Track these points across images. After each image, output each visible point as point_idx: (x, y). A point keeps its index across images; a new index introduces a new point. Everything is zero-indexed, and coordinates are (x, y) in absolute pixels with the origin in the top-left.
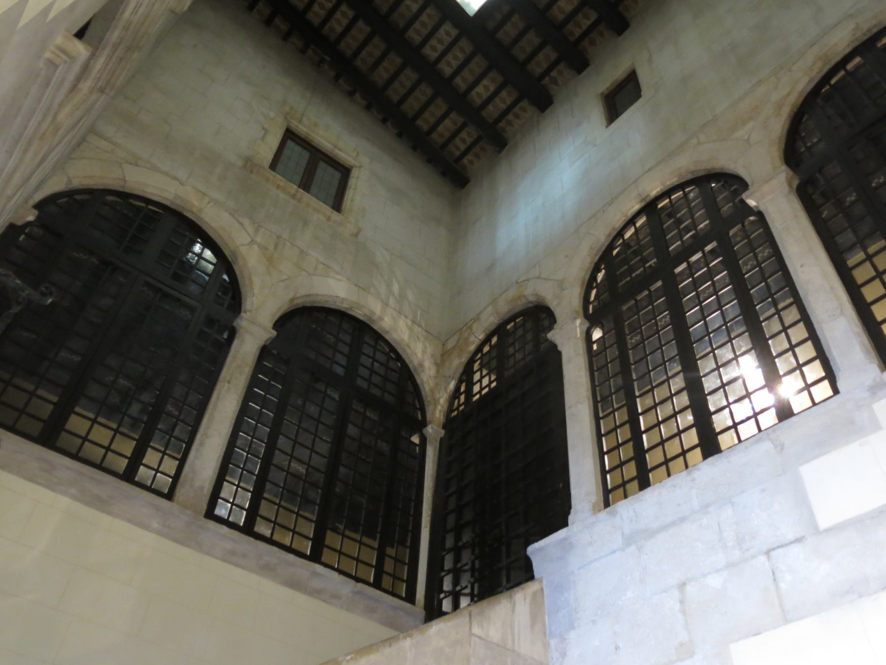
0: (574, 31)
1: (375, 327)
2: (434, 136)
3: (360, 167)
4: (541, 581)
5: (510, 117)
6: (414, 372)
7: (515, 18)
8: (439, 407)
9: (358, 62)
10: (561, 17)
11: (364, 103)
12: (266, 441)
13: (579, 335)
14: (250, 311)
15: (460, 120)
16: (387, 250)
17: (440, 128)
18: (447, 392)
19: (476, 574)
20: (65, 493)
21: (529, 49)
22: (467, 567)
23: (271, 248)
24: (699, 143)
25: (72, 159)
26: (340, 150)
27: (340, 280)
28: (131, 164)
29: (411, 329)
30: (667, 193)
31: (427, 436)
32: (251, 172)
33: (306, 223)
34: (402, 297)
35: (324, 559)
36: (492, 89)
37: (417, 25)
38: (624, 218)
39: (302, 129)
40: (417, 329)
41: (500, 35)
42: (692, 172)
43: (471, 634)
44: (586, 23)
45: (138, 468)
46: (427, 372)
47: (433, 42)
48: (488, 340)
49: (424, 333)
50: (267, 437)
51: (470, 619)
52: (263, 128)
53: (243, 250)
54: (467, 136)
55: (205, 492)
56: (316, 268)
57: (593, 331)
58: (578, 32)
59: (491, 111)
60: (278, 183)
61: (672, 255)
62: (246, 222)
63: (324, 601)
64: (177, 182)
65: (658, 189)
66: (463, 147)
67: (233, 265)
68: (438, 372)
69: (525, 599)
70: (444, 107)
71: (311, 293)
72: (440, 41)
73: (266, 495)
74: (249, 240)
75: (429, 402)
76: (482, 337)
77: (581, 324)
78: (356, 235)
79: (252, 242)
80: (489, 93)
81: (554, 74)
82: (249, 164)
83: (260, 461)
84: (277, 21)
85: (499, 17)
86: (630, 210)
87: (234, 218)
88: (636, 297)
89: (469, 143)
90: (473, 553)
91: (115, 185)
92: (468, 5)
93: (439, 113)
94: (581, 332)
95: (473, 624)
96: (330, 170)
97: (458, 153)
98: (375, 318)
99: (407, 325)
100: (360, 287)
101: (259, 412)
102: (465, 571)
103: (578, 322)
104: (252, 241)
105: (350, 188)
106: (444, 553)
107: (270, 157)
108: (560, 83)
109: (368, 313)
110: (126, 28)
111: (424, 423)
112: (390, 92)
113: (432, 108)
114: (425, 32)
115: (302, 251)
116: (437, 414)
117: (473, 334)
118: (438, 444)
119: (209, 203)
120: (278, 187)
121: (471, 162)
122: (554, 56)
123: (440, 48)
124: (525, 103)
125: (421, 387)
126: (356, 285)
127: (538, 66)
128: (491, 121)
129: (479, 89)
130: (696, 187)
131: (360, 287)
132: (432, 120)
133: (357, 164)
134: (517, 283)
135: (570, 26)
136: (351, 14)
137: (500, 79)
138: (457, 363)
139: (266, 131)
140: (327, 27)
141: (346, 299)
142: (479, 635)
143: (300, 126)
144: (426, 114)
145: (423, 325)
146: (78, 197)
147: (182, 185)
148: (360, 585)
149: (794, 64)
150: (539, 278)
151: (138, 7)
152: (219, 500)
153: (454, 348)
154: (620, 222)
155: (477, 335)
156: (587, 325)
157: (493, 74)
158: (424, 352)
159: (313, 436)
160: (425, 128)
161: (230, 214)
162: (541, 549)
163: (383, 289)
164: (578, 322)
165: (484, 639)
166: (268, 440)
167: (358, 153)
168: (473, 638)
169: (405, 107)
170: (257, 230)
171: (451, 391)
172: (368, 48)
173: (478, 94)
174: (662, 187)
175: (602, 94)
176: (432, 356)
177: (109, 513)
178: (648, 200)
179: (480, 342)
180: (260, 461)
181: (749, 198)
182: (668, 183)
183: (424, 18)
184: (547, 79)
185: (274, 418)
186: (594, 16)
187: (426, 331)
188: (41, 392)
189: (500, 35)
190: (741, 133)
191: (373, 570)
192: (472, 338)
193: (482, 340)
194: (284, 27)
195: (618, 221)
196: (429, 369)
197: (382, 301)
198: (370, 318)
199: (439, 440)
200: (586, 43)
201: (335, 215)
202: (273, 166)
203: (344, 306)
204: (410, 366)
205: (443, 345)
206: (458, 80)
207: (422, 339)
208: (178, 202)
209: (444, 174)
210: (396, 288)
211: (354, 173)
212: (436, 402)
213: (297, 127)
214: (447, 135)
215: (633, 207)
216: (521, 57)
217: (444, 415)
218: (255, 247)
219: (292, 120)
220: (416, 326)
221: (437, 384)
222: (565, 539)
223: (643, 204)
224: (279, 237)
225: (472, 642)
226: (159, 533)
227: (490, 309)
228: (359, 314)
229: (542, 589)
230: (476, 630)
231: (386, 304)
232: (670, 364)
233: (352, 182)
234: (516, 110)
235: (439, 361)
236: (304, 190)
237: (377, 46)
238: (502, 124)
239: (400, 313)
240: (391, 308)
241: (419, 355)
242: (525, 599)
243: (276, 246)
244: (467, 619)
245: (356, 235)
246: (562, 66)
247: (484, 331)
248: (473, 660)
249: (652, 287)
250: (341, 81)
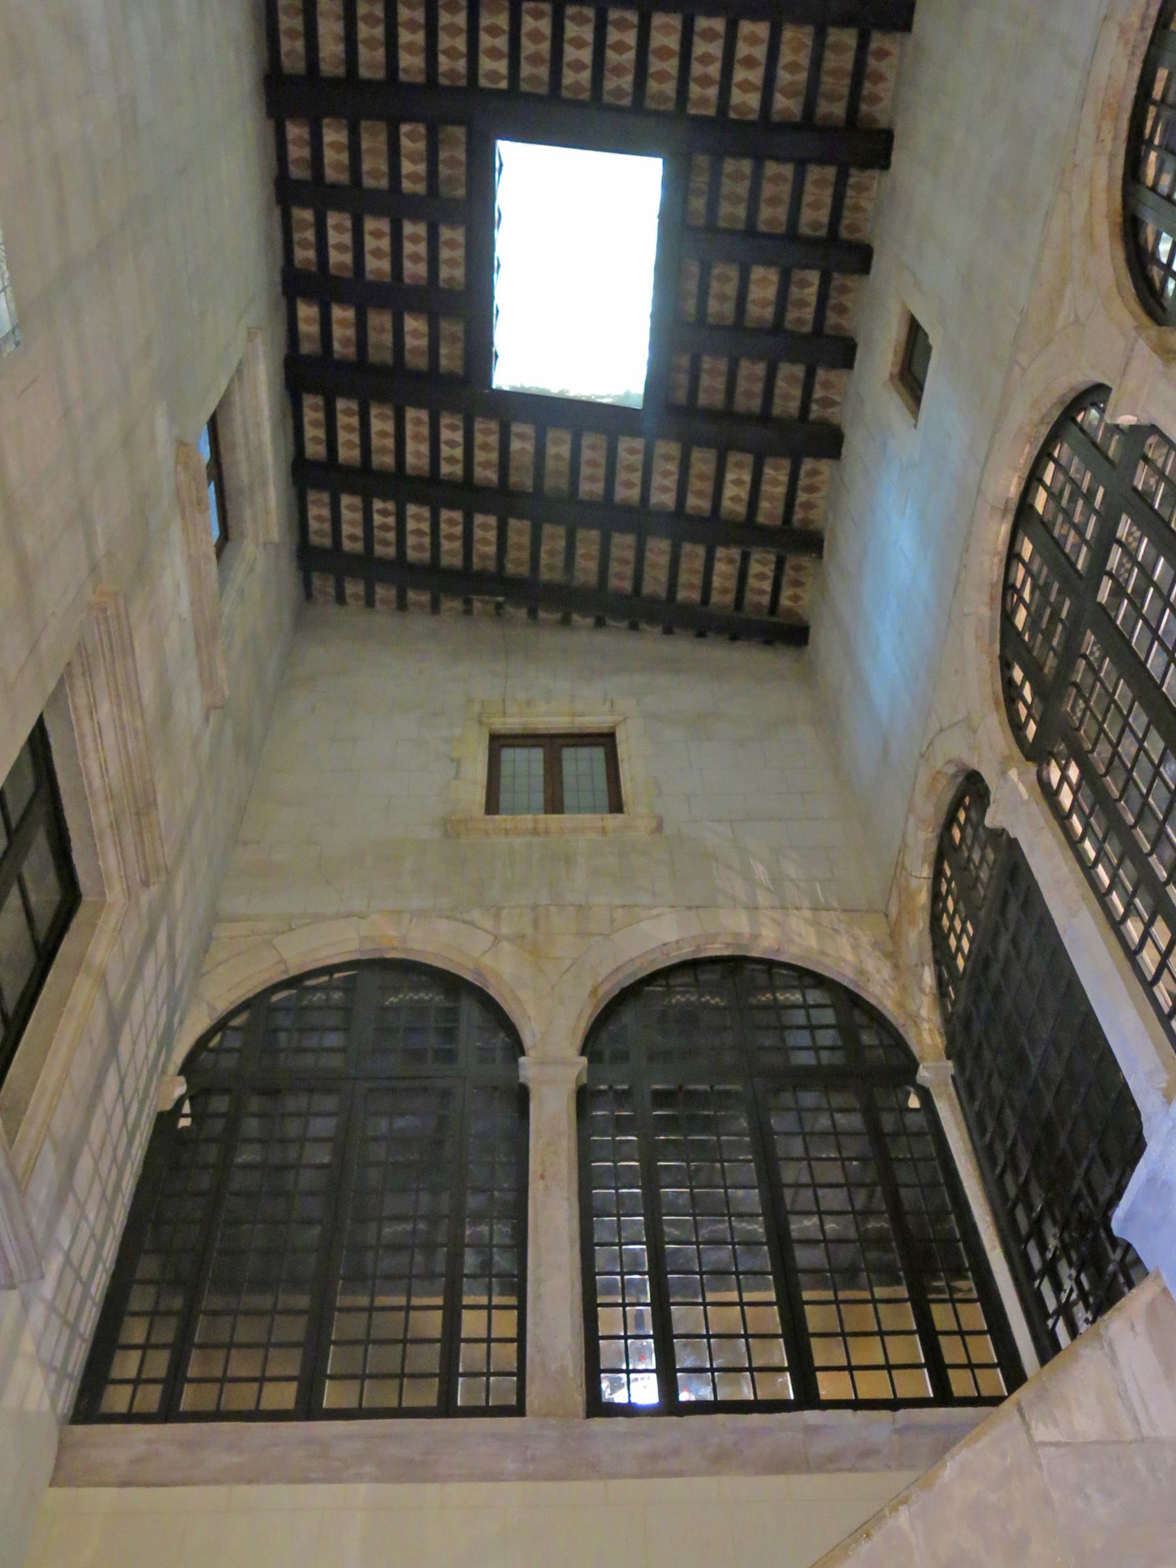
0: (801, 316)
1: (755, 954)
2: (715, 598)
3: (625, 720)
4: (1158, 1276)
5: (802, 497)
6: (856, 990)
7: (707, 363)
8: (926, 1026)
9: (545, 575)
10: (769, 313)
11: (590, 621)
12: (644, 1240)
13: (1026, 796)
14: (534, 1047)
15: (735, 553)
16: (719, 821)
17: (717, 582)
18: (926, 994)
19: (1091, 1300)
20: (359, 1478)
21: (758, 387)
22: (1074, 1296)
23: (529, 930)
24: (1024, 370)
25: (203, 975)
26: (582, 715)
27: (658, 916)
28: (283, 932)
29: (816, 924)
30: (1033, 479)
31: (927, 1085)
32: (458, 836)
33: (569, 860)
34: (777, 879)
35: (825, 1393)
36: (747, 478)
37: (585, 471)
38: (996, 560)
39: (512, 723)
40: (825, 917)
41: (703, 399)
42: (1042, 421)
43: (1035, 1446)
44: (811, 293)
45: (777, 1295)
46: (877, 976)
47: (622, 476)
48: (938, 873)
49: (843, 917)
50: (644, 1232)
51: (1022, 1416)
52: (452, 760)
53: (487, 961)
54: (761, 566)
55: (571, 1374)
56: (612, 920)
57: (1048, 773)
58: (809, 313)
59: (770, 510)
60: (504, 826)
61: (1084, 575)
62: (476, 915)
63: (852, 1470)
64: (355, 919)
65: (1015, 480)
66: (767, 586)
67: (486, 990)
68: (896, 967)
69: (1132, 1327)
70: (701, 551)
71: (619, 964)
72: (630, 468)
73: (807, 1295)
74: (491, 938)
75: (904, 1025)
76: (926, 871)
77: (1020, 775)
78: (659, 828)
79: (497, 939)
80: (748, 487)
81: (818, 393)
82: (451, 827)
83: (647, 1277)
84: (412, 595)
85: (683, 379)
86: (998, 539)
87: (456, 920)
88: (1073, 679)
89: (771, 574)
90: (1071, 1264)
91: (277, 975)
92: (627, 395)
93: (699, 564)
94: (1030, 790)
95: (1033, 1424)
96: (583, 752)
97: (766, 600)
98: (744, 941)
99: (806, 920)
100: (698, 907)
101: (615, 1198)
102: (1075, 1303)
103: (1013, 774)
104: (496, 937)
105: (622, 761)
106: (1038, 1282)
107: (480, 795)
108: (837, 398)
109: (730, 940)
110: (110, 796)
111: (912, 1065)
112: (613, 583)
113: (684, 565)
114: (601, 472)
115: (580, 906)
116: (927, 1038)
117: (911, 875)
118: (952, 1089)
119: (411, 919)
120: (507, 832)
121: (796, 598)
122: (799, 370)
123: (636, 477)
124: (808, 464)
125: (880, 1008)
126: (689, 908)
127: (787, 402)
128: (779, 522)
129: (730, 491)
130: (1062, 443)
131: (698, 907)
132: (697, 580)
133: (619, 718)
134: (922, 756)
135: (791, 315)
136: (492, 520)
137: (749, 459)
138: (917, 935)
139: (457, 761)
140: (475, 560)
141: (683, 939)
142: (1054, 1440)
143: (509, 720)
144: (683, 578)
145: (835, 905)
146: (237, 1021)
147: (363, 918)
148: (902, 1414)
149: (1074, 152)
150: (941, 730)
151: (103, 764)
152: (490, 1404)
153: (899, 914)
154: (995, 568)
155: (918, 874)
156: (1032, 768)
157: (733, 458)
158: (856, 947)
159: (805, 1163)
160: (695, 596)
161: (448, 918)
162: (1130, 1217)
163: (739, 889)
164: (1013, 774)
165: (1066, 1444)
166: (647, 1236)
167: (612, 703)
168: (1040, 1451)
169: (648, 588)
170: (497, 917)
171: (931, 988)
172: (544, 548)
173: (732, 499)
174: (1018, 474)
175: (892, 377)
176: (875, 945)
177: (434, 1479)
178: (1013, 506)
179: (930, 881)
180: (647, 1277)
181: (1116, 417)
182: (1022, 461)
183: (586, 454)
184: (814, 407)
185: (643, 1193)
186: (814, 277)
187: (845, 911)
188: (381, 1301)
189: (703, 399)
190: (1064, 316)
191: (925, 1370)
192: (914, 883)
193: (932, 876)
194: (425, 598)
195: (992, 569)
196: (879, 971)
197: (746, 908)
198: (738, 945)
199: (950, 1081)
200: (832, 318)
201: (612, 821)
202: (492, 807)
203: (686, 952)
204: (845, 983)
205: (886, 916)
206: (692, 501)
207: (842, 927)
208: (369, 945)
209: (768, 642)
210: (761, 872)
211: (620, 737)
212: (915, 1019)
213: (505, 723)
214: (732, 584)
215: (999, 531)
216: (756, 405)
217: (940, 1033)
218: (505, 945)
219: (492, 720)
220: (824, 913)
221: (904, 988)
222: (1151, 1179)
223: (1010, 518)
224: (534, 907)
225: (1043, 1462)
226: (523, 1477)
227: (912, 821)
228: (716, 949)
229: (1165, 1291)
230: (1042, 1432)
231: (754, 909)
232: (1165, 768)
233: (622, 750)
234: (803, 481)
235: (889, 948)
236: (554, 812)
237: (554, 538)
238: (798, 515)
239: (784, 908)
240: (766, 908)
241: (850, 957)
242: (1132, 1327)
243: (535, 924)
244: (1017, 1419)
245: (659, 828)
246: (821, 374)
247: (923, 862)
248: (1056, 1495)
249: (1084, 647)
250: (542, 614)
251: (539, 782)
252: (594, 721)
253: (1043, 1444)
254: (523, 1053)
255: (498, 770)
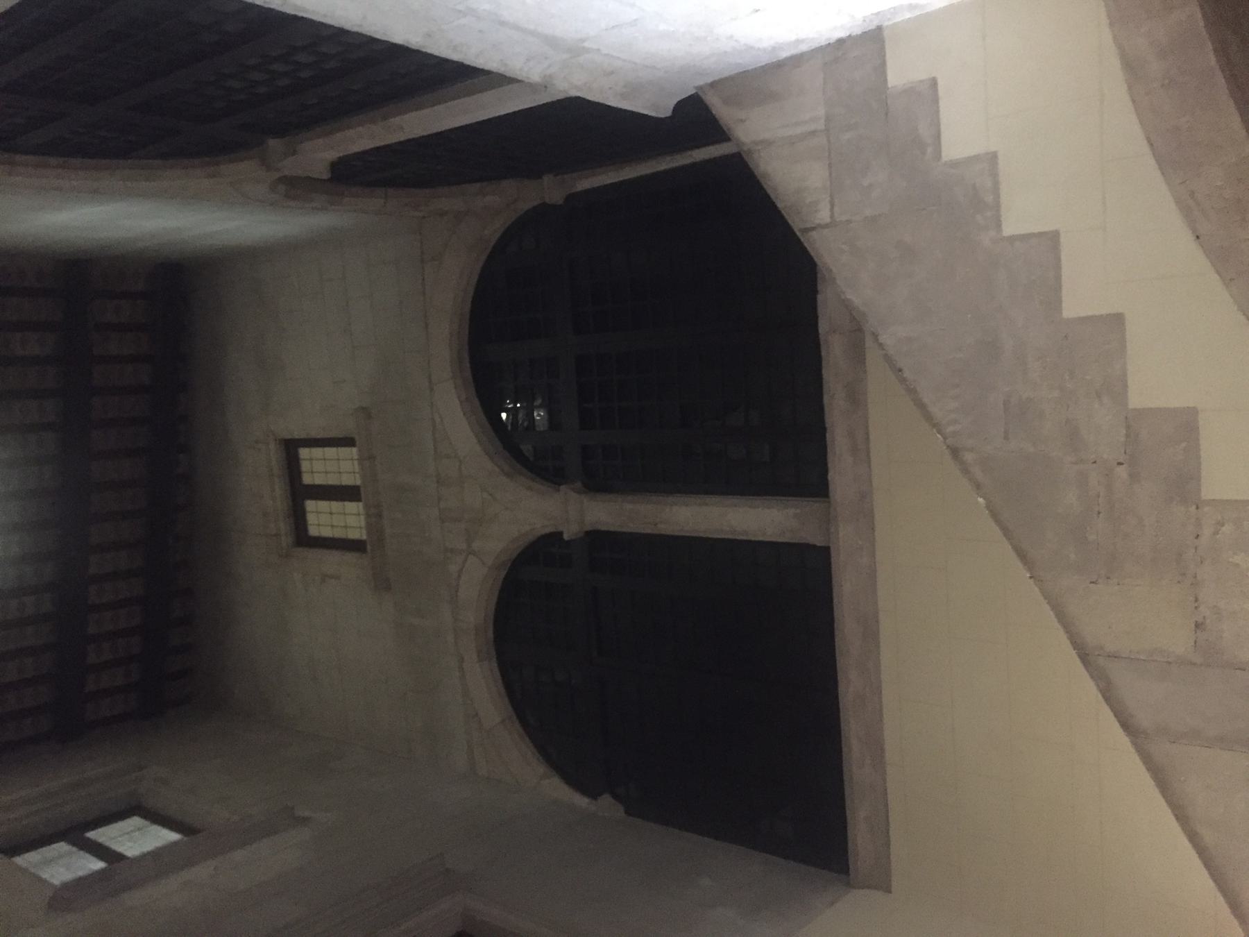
39: (284, 526)
62: (453, 568)
95: (817, 222)
100: (430, 382)
104: (470, 553)
126: (432, 390)
161: (457, 591)
165: (832, 196)
204: (481, 264)
244: (814, 233)
251: (335, 506)
252: (273, 456)
253: (832, 216)
254: (561, 533)
255: (325, 539)
